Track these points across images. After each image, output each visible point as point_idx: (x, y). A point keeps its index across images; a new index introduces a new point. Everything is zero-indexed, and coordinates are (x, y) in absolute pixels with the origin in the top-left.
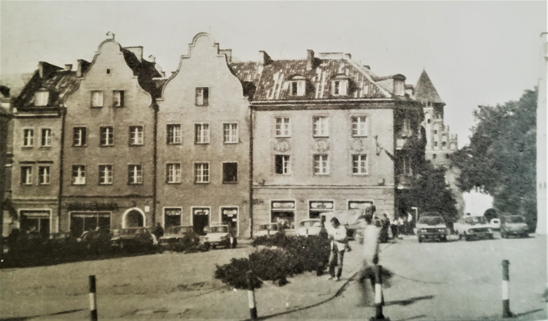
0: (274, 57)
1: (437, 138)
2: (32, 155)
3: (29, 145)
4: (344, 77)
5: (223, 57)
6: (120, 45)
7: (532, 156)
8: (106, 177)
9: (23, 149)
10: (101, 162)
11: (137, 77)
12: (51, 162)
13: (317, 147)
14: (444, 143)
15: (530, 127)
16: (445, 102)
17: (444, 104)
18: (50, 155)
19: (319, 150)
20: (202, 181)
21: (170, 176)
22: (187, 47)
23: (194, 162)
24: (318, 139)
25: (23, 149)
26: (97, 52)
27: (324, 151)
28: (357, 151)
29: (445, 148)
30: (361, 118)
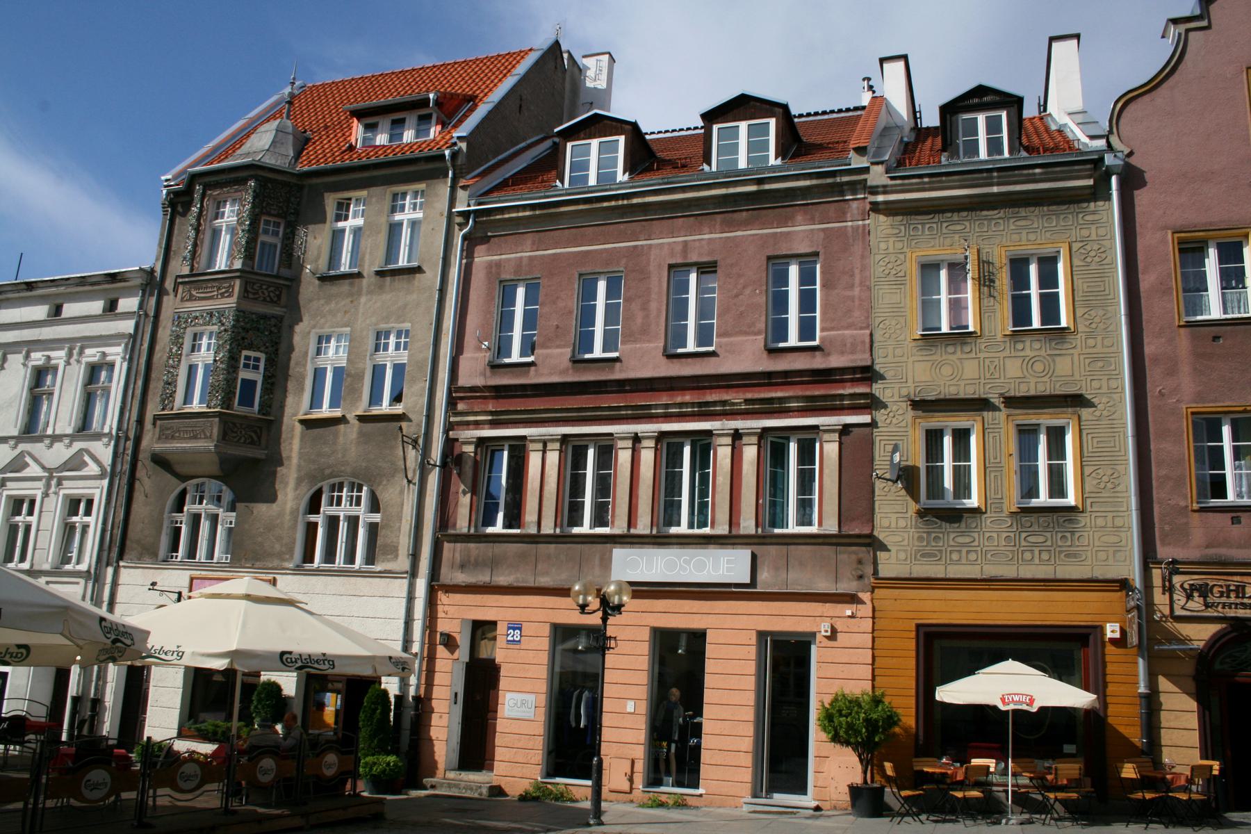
12: (1076, 401)
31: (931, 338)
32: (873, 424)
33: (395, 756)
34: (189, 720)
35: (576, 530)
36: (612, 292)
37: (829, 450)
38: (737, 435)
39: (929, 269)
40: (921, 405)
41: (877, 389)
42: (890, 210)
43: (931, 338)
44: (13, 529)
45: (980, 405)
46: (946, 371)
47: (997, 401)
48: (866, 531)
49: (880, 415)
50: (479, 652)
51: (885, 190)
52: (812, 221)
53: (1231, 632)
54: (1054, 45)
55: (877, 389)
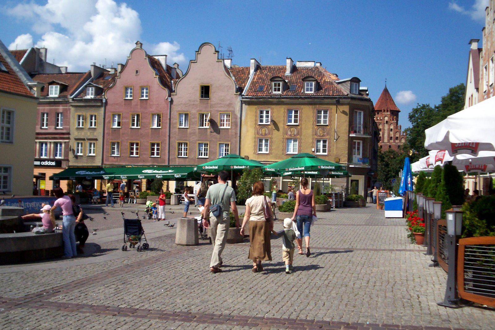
0: (263, 65)
1: (392, 134)
2: (83, 134)
3: (81, 126)
4: (313, 79)
5: (221, 62)
6: (146, 52)
7: (460, 110)
8: (135, 151)
9: (78, 129)
10: (131, 140)
11: (158, 77)
12: (96, 140)
13: (289, 133)
14: (397, 138)
15: (456, 300)
16: (400, 110)
17: (399, 111)
18: (95, 134)
19: (291, 135)
20: (183, 156)
21: (180, 152)
22: (194, 53)
23: (177, 142)
24: (290, 127)
25: (78, 129)
26: (129, 57)
27: (295, 136)
28: (319, 136)
29: (397, 141)
30: (324, 111)
31: (78, 129)
32: (69, 142)
33: (66, 191)
34: (181, 203)
35: (113, 155)
36: (47, 116)
37: (63, 145)
38: (50, 143)
39: (79, 116)
40: (76, 139)
41: (70, 136)
42: (72, 106)
43: (78, 129)
44: (179, 148)
45: (84, 140)
46: (80, 133)
47: (86, 140)
48: (67, 158)
49: (70, 141)
50: (453, 216)
51: (72, 103)
52: (63, 106)
53: (446, 212)
54: (198, 51)
55: (70, 136)
